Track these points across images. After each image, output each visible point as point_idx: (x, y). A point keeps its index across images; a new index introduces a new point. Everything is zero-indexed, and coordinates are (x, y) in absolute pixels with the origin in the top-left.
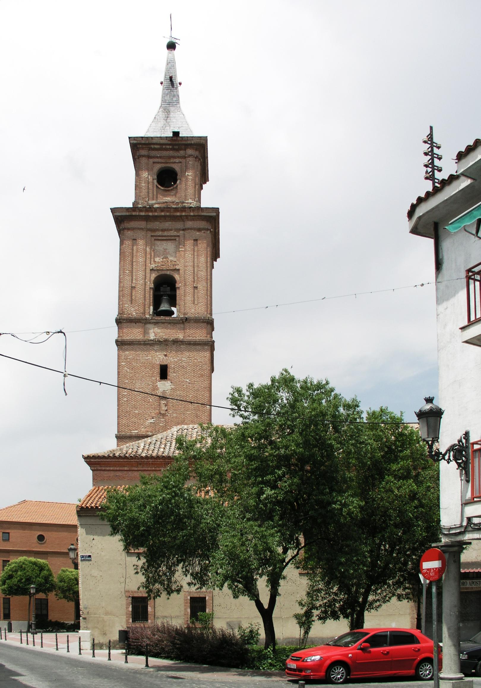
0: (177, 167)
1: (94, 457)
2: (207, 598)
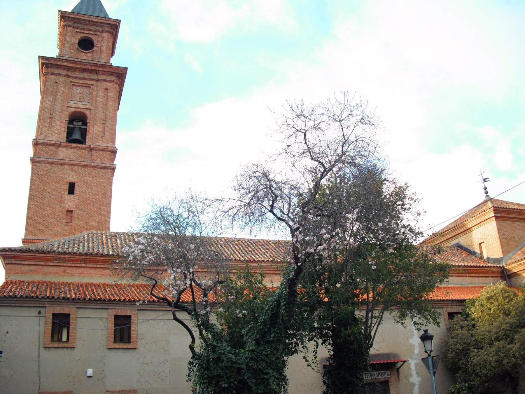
0: (94, 38)
1: (10, 250)
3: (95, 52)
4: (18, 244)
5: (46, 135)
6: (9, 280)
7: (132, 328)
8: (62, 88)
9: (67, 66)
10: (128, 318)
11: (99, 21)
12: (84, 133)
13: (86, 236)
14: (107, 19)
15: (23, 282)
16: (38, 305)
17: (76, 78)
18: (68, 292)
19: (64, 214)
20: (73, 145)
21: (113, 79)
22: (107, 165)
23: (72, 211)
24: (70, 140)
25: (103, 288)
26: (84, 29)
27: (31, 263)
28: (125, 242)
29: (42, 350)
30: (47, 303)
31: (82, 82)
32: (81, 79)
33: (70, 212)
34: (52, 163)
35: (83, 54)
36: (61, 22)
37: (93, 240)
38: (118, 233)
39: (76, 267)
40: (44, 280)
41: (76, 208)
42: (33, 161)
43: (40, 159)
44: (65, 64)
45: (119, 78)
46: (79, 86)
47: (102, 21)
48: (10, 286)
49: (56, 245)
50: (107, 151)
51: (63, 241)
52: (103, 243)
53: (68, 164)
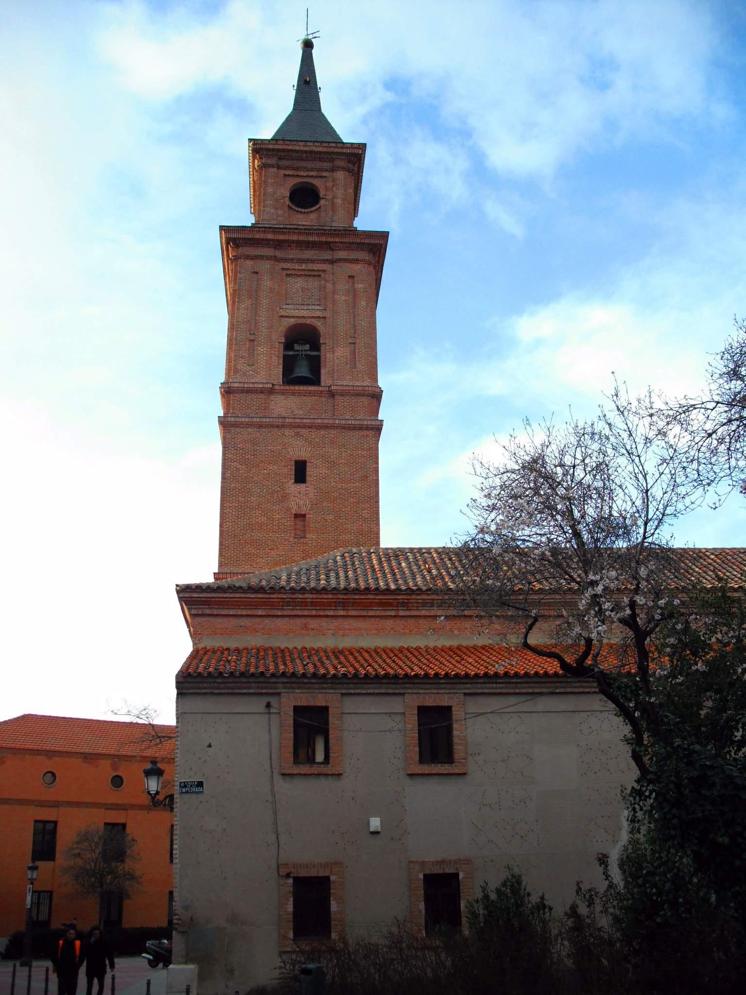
0: (317, 182)
2: (461, 876)
3: (322, 209)
4: (211, 579)
5: (245, 374)
6: (200, 646)
7: (455, 733)
8: (267, 283)
9: (272, 240)
10: (445, 712)
11: (325, 150)
12: (315, 365)
13: (338, 558)
14: (340, 145)
15: (228, 649)
16: (264, 691)
17: (292, 260)
18: (318, 664)
19: (289, 523)
20: (297, 388)
21: (363, 255)
22: (366, 423)
23: (304, 516)
24: (290, 377)
25: (385, 656)
26: (298, 169)
27: (239, 612)
28: (417, 565)
29: (277, 778)
30: (280, 685)
31: (304, 267)
32: (301, 261)
33: (300, 516)
34: (260, 426)
35: (301, 216)
36: (254, 162)
37: (353, 564)
38: (400, 549)
39: (327, 616)
40: (267, 645)
41: (311, 509)
42: (224, 423)
43: (237, 419)
44: (270, 236)
45: (374, 254)
46: (300, 276)
47: (330, 150)
48: (206, 658)
49: (284, 577)
50: (363, 395)
51: (295, 569)
52: (374, 570)
53: (291, 426)
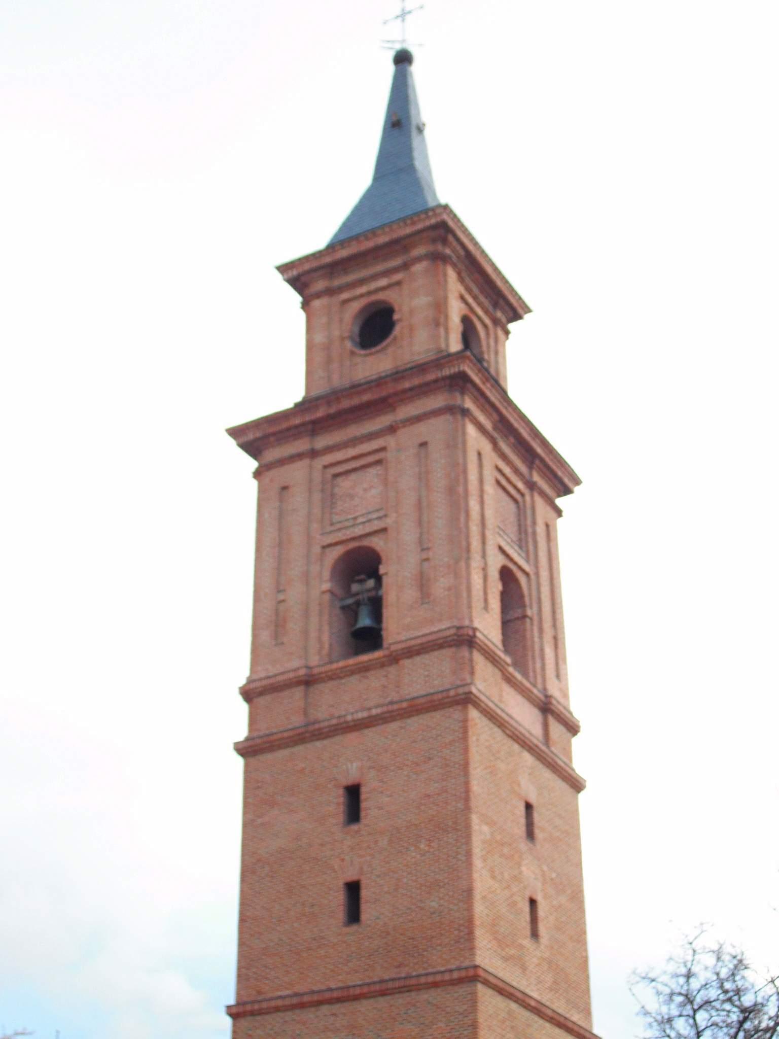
0: (390, 296)
